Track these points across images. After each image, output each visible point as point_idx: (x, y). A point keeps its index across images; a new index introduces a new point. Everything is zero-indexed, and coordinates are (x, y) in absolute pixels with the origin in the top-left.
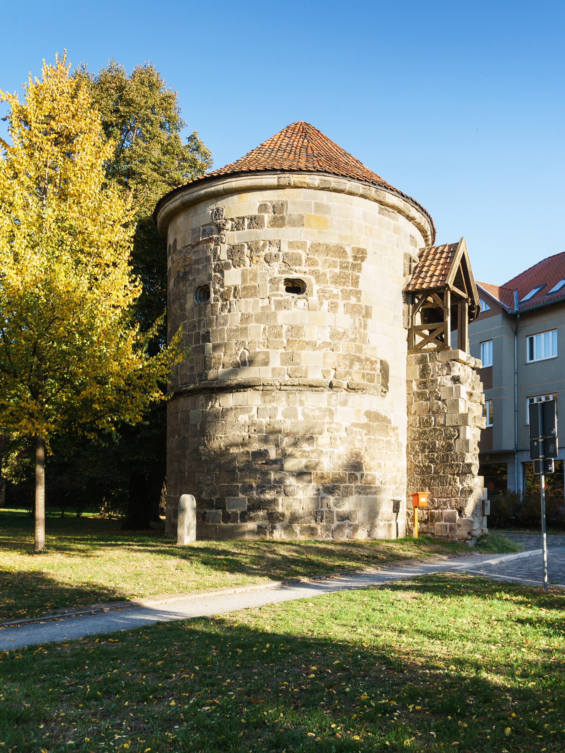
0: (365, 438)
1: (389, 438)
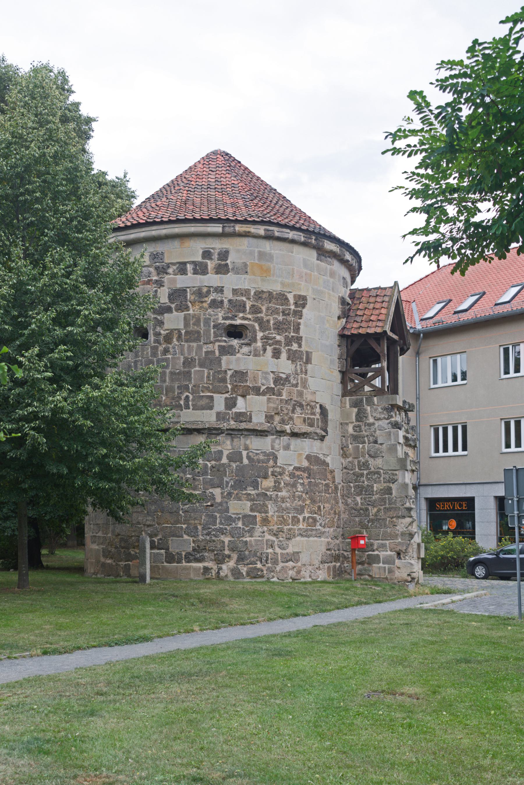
0: (306, 481)
1: (327, 482)
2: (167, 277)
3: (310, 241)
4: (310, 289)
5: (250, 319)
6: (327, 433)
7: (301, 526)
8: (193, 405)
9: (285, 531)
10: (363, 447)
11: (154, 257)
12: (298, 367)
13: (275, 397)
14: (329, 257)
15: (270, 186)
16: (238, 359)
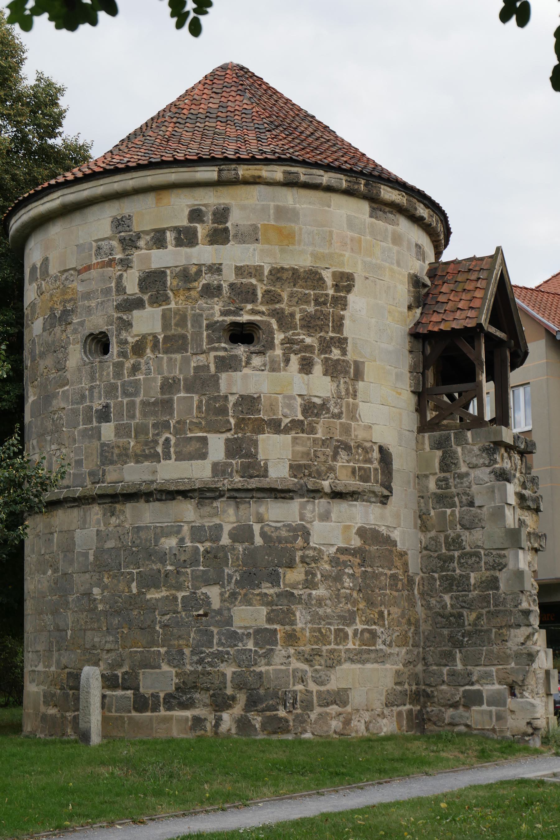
0: (359, 571)
2: (137, 253)
3: (356, 187)
4: (360, 262)
5: (263, 313)
6: (391, 492)
7: (350, 646)
8: (176, 453)
9: (324, 654)
10: (453, 513)
11: (120, 223)
12: (342, 386)
13: (305, 435)
14: (391, 213)
15: (306, 112)
16: (246, 376)
